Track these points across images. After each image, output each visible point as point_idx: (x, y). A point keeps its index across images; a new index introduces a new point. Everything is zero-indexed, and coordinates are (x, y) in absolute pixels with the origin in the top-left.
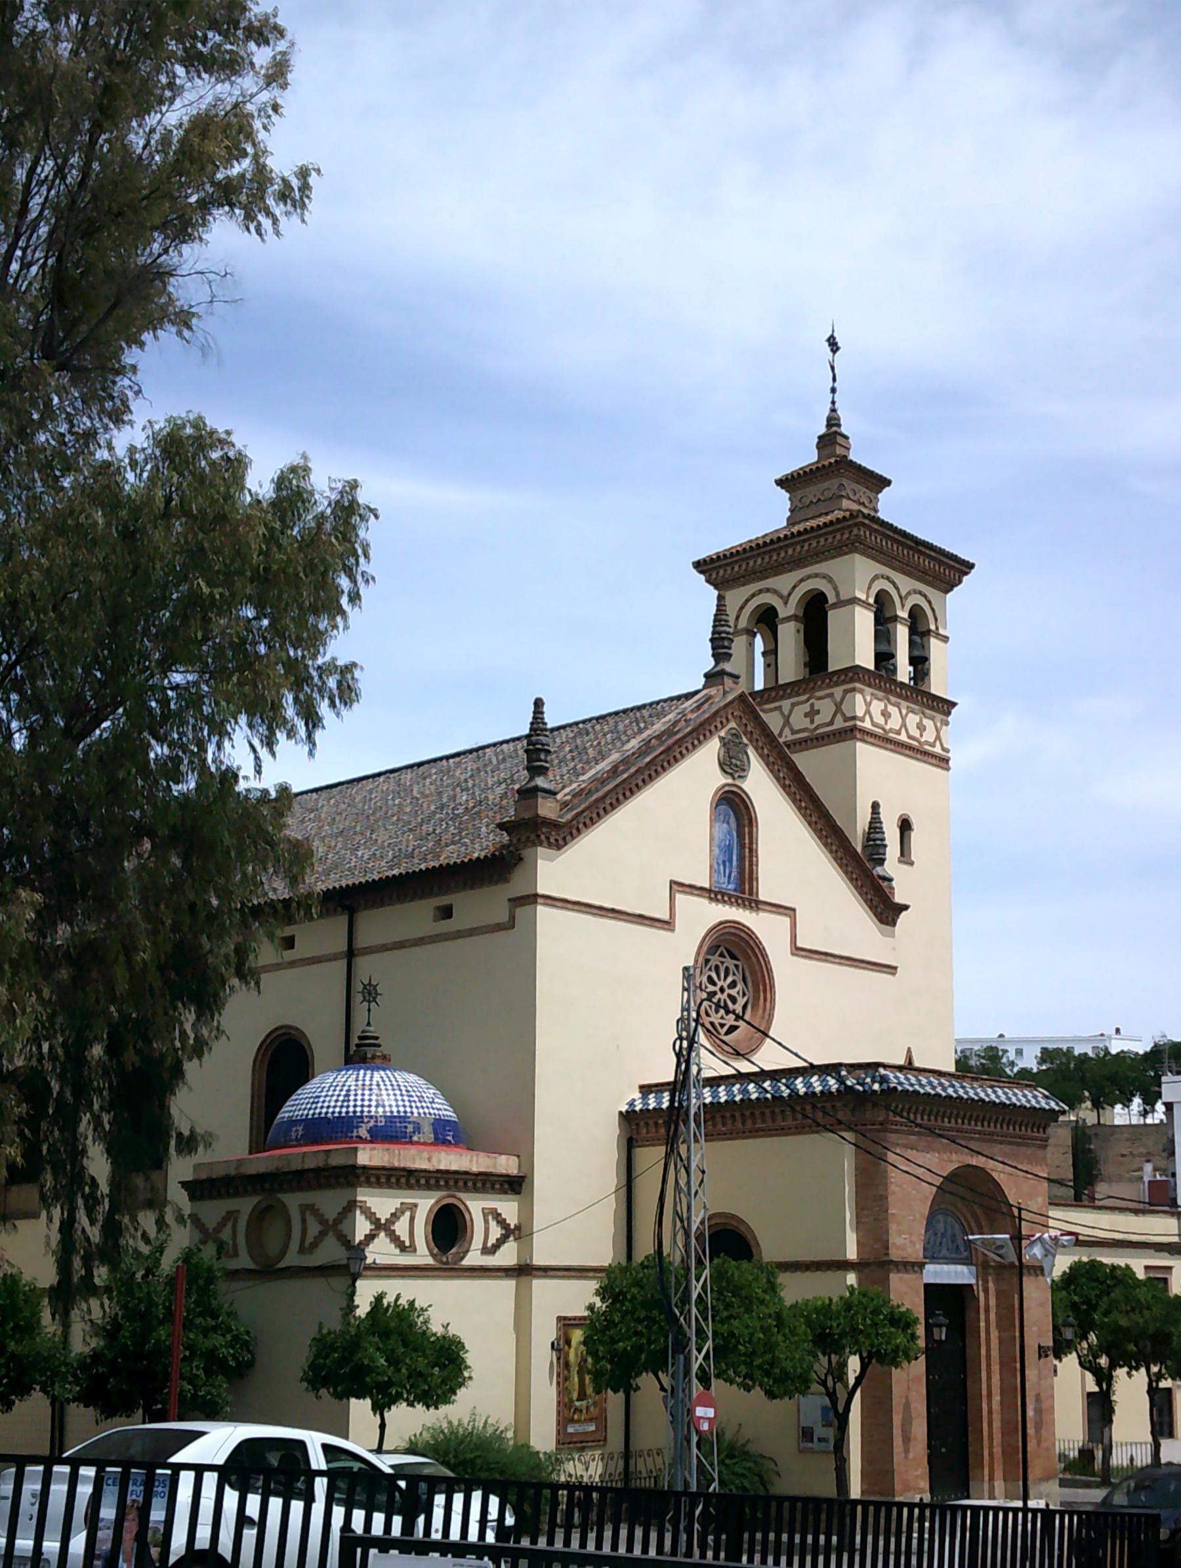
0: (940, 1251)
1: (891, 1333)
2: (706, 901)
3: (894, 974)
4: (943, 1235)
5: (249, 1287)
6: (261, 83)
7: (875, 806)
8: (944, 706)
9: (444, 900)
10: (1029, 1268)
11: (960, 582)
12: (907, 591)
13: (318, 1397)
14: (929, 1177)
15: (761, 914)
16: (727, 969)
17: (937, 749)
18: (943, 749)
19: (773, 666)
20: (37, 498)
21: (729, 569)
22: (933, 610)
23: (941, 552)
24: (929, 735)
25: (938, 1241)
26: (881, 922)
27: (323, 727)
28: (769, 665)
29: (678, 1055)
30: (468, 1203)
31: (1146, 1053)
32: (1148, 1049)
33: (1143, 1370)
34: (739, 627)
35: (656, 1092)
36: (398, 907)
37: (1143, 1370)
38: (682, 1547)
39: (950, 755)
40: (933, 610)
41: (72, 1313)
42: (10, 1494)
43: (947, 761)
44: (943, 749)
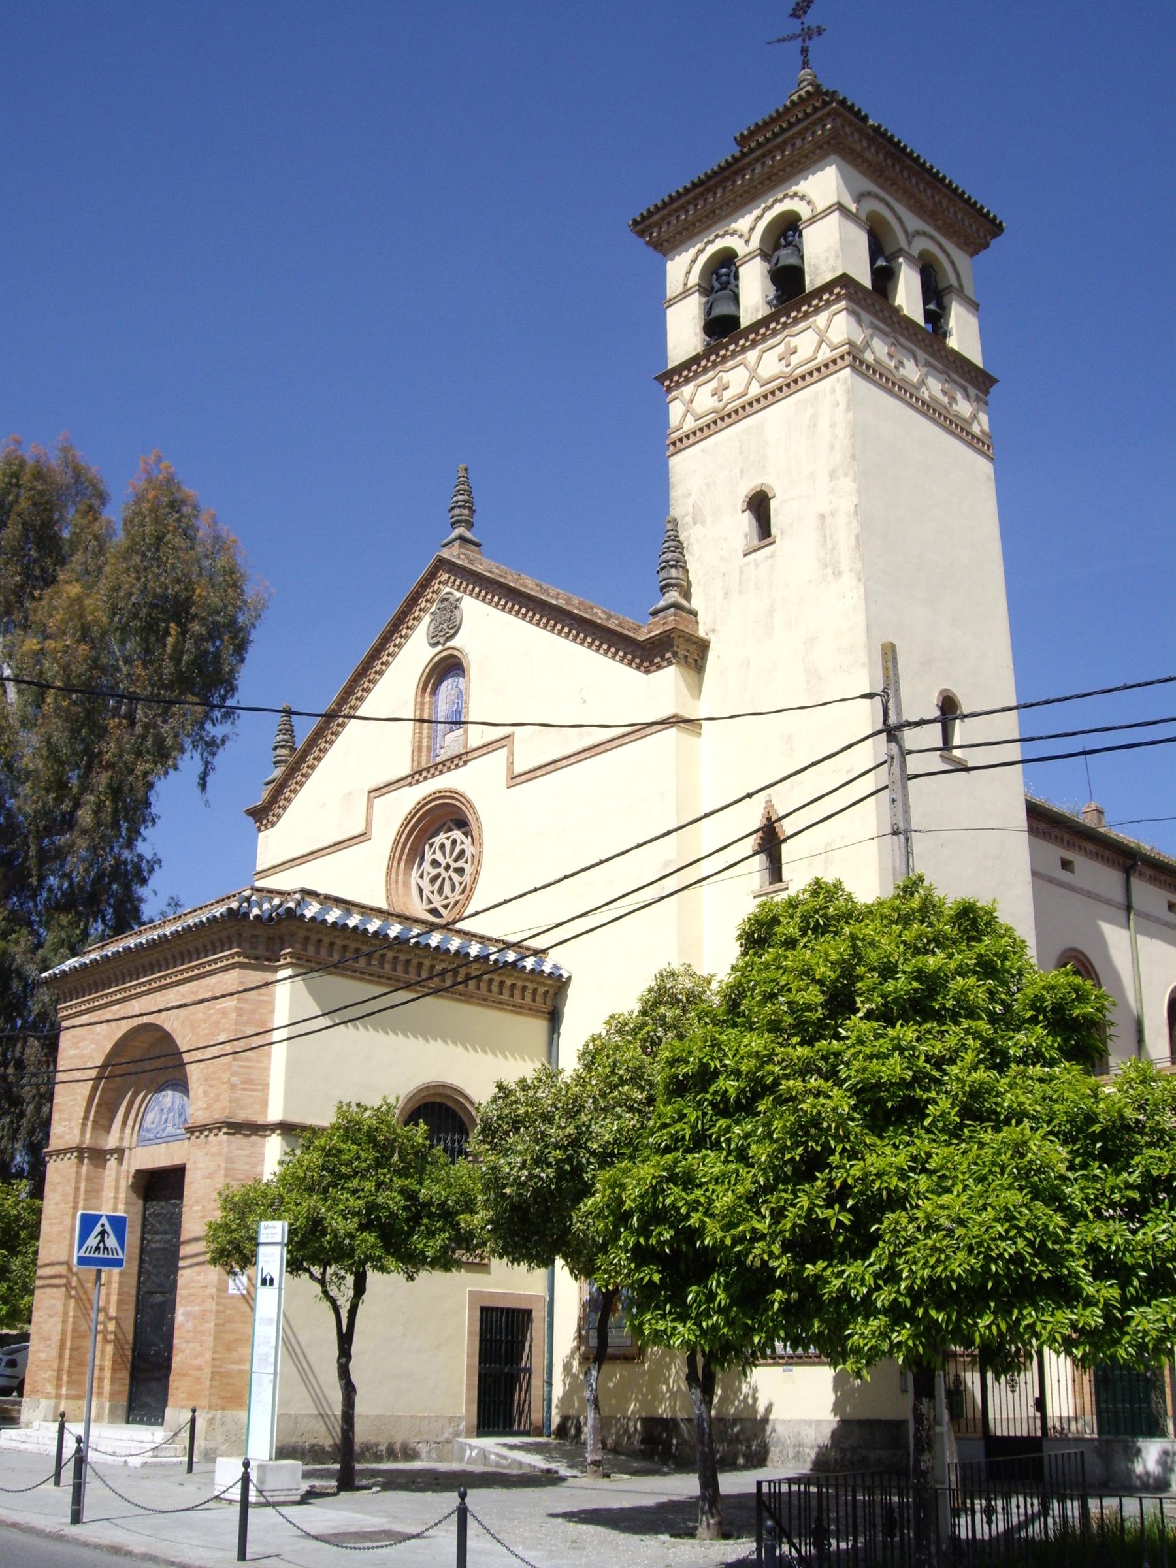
0: (164, 1130)
1: (344, 1142)
3: (239, 1559)
4: (170, 1110)
5: (386, 1546)
7: (755, 897)
9: (1069, 855)
10: (43, 693)
13: (769, 1409)
14: (198, 1055)
16: (463, 852)
19: (899, 804)
20: (69, 822)
21: (691, 207)
22: (953, 263)
23: (956, 194)
25: (164, 1117)
27: (411, 1278)
28: (894, 801)
29: (466, 763)
30: (754, 836)
32: (866, 236)
34: (690, 285)
35: (362, 914)
36: (519, 1490)
41: (445, 683)
42: (238, 1498)
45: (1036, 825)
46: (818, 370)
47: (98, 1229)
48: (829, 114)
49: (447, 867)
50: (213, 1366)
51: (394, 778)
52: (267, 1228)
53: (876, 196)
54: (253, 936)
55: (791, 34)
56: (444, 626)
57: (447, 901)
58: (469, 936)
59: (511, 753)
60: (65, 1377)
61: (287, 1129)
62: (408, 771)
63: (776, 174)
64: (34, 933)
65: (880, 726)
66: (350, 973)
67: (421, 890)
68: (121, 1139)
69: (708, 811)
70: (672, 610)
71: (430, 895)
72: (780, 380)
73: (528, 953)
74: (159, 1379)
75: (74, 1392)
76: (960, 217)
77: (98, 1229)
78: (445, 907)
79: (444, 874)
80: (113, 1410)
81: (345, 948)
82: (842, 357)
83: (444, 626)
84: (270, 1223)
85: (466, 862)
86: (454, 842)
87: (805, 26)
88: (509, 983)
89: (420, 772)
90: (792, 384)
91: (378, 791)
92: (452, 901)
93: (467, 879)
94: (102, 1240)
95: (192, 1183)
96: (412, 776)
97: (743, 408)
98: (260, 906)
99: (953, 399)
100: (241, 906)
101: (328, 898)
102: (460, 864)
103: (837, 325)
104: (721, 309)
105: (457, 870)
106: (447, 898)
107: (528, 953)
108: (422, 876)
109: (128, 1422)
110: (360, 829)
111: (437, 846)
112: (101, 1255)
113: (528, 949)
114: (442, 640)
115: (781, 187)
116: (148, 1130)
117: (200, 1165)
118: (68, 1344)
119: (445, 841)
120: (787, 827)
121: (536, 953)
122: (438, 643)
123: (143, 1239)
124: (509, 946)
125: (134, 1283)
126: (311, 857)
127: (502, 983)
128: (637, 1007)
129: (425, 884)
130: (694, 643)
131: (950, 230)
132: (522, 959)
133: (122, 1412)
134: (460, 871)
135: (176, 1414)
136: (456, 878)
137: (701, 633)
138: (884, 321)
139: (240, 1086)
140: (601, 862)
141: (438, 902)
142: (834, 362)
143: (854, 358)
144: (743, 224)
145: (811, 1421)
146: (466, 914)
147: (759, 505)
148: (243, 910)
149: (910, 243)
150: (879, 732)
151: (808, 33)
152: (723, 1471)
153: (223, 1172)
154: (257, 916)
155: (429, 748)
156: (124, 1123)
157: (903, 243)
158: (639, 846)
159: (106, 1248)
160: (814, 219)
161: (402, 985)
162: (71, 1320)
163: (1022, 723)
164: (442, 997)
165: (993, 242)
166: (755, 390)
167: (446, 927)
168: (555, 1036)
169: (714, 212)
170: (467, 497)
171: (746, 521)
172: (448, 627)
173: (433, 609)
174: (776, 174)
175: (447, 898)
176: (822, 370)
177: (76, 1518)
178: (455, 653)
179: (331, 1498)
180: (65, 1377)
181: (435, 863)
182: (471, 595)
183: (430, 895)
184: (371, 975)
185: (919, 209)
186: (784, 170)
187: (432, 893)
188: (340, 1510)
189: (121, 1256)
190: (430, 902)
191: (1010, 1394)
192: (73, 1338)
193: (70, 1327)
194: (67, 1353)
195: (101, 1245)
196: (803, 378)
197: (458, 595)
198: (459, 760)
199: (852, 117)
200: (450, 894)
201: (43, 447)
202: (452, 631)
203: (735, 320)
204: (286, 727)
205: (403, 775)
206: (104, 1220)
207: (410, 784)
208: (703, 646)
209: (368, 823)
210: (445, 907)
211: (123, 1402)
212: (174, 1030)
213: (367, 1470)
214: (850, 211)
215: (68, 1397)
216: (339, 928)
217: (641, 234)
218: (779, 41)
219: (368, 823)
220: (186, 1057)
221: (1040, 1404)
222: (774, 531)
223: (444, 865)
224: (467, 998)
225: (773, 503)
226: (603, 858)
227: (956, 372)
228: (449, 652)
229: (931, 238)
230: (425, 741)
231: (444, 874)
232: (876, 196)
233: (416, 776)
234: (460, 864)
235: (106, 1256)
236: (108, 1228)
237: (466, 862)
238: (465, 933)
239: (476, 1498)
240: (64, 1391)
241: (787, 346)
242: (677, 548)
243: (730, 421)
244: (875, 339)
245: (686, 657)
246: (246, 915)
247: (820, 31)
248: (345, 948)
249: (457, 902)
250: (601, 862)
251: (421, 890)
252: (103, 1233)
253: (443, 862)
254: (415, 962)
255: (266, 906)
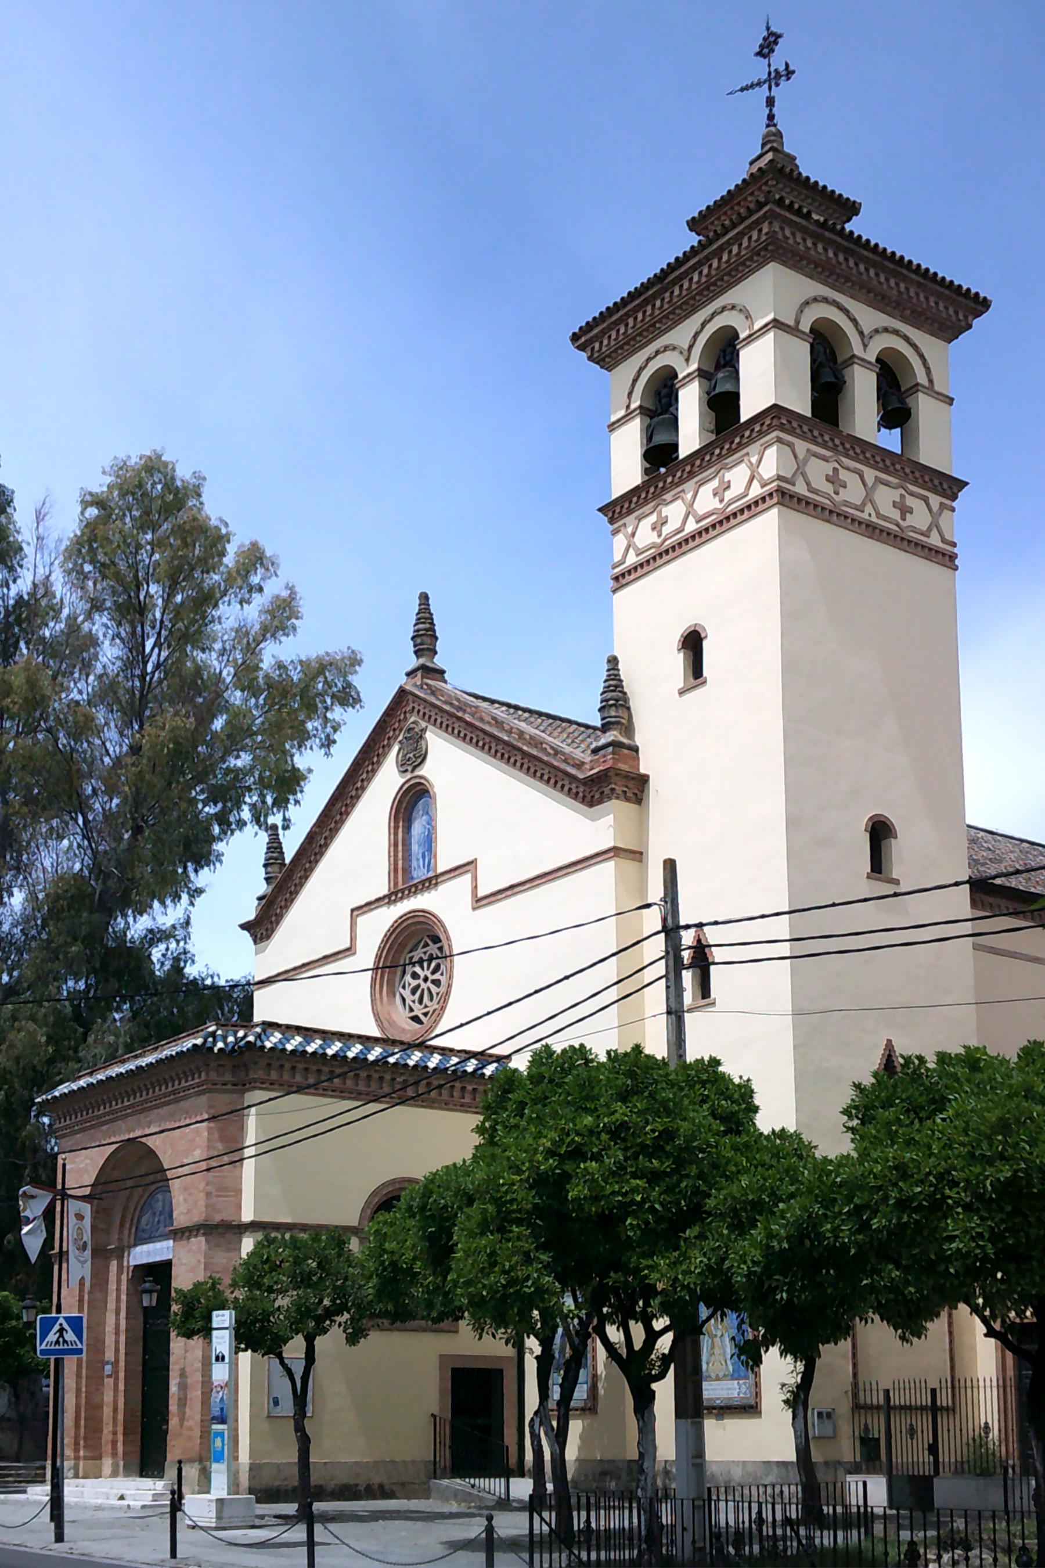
2: (385, 909)
6: (36, 582)
8: (949, 487)
11: (970, 327)
12: (869, 330)
15: (441, 888)
17: (934, 540)
18: (944, 540)
22: (922, 356)
24: (919, 518)
26: (591, 804)
30: (909, 386)
31: (843, 377)
33: (481, 1118)
37: (481, 1118)
38: (860, 1485)
39: (955, 550)
40: (922, 356)
43: (953, 557)
44: (944, 540)
45: (977, 896)
46: (853, 520)
47: (57, 1327)
48: (765, 217)
49: (426, 979)
50: (202, 1427)
51: (373, 898)
52: (217, 1316)
53: (826, 300)
54: (219, 1065)
55: (756, 81)
56: (411, 755)
57: (425, 950)
58: (446, 1052)
59: (475, 879)
60: (82, 1442)
61: (254, 1226)
62: (386, 892)
63: (714, 284)
64: (103, 809)
65: (660, 928)
66: (258, 1084)
67: (404, 1000)
68: (120, 1239)
69: (538, 988)
70: (610, 749)
71: (412, 1004)
72: (653, 550)
73: (490, 1059)
74: (235, 1249)
75: (90, 1454)
76: (941, 308)
77: (57, 1327)
78: (425, 1014)
79: (423, 985)
80: (126, 1467)
81: (319, 1071)
82: (771, 495)
83: (411, 755)
84: (220, 1312)
85: (442, 974)
86: (421, 1001)
87: (772, 69)
88: (470, 1088)
89: (395, 893)
90: (725, 521)
91: (358, 911)
92: (431, 1009)
93: (443, 989)
94: (61, 1335)
95: (177, 1276)
96: (388, 896)
97: (680, 544)
98: (224, 1038)
99: (558, 1370)
100: (205, 1041)
101: (289, 1027)
102: (437, 976)
103: (769, 461)
104: (660, 439)
105: (434, 982)
106: (426, 1006)
107: (490, 1059)
108: (404, 987)
109: (141, 1476)
110: (348, 945)
111: (308, 746)
112: (61, 1347)
113: (491, 1056)
114: (410, 768)
115: (164, 1111)
116: (143, 1231)
117: (184, 1261)
118: (83, 1415)
119: (429, 1004)
120: (718, 954)
121: (499, 1059)
122: (406, 771)
123: (145, 1324)
124: (474, 1055)
125: (140, 1361)
126: (509, 893)
127: (463, 1089)
128: (469, 1156)
129: (407, 993)
130: (633, 778)
131: (921, 319)
132: (483, 1067)
133: (136, 1467)
134: (437, 983)
135: (171, 1473)
136: (434, 989)
137: (643, 770)
138: (824, 445)
139: (215, 1193)
140: (462, 1025)
141: (418, 1011)
142: (763, 499)
143: (784, 496)
144: (681, 334)
145: (738, 1462)
146: (437, 1031)
147: (693, 643)
148: (208, 1045)
149: (865, 346)
150: (658, 933)
151: (775, 78)
152: (514, 1477)
153: (202, 1266)
154: (220, 1050)
155: (403, 869)
156: (122, 1225)
157: (857, 349)
158: (489, 1013)
159: (65, 1341)
160: (751, 338)
161: (294, 1089)
162: (84, 1395)
163: (243, 1154)
164: (409, 1105)
165: (976, 322)
166: (691, 526)
167: (421, 1046)
168: (418, 828)
169: (653, 325)
170: (428, 626)
171: (677, 662)
172: (414, 757)
173: (400, 738)
174: (714, 284)
175: (426, 1006)
176: (752, 509)
177: (59, 1538)
178: (422, 781)
179: (358, 1525)
180: (82, 1442)
181: (415, 976)
182: (435, 724)
183: (412, 1004)
184: (333, 1091)
185: (881, 302)
186: (722, 279)
187: (414, 1002)
188: (1003, 1387)
189: (80, 1346)
190: (411, 1010)
191: (909, 1440)
192: (86, 1409)
193: (83, 1402)
194: (82, 1422)
195: (61, 1340)
196: (735, 515)
197: (423, 724)
198: (431, 883)
199: (938, 287)
200: (429, 1004)
201: (10, 485)
202: (419, 760)
203: (675, 447)
204: (275, 845)
205: (381, 895)
206: (61, 1321)
207: (389, 903)
208: (644, 780)
209: (353, 939)
210: (425, 1014)
211: (136, 1459)
212: (156, 1147)
213: (753, 222)
214: (789, 326)
215: (85, 1458)
216: (299, 1054)
217: (582, 348)
218: (742, 90)
219: (353, 939)
220: (170, 1174)
221: (933, 1449)
222: (706, 672)
223: (422, 976)
224: (431, 1105)
225: (705, 643)
226: (464, 1022)
227: (915, 483)
228: (418, 780)
229: (896, 332)
230: (400, 863)
231: (423, 985)
232: (826, 300)
233: (392, 897)
234: (437, 976)
235: (66, 1347)
236: (66, 1326)
237: (442, 974)
238: (443, 1049)
239: (305, 1549)
240: (82, 1453)
241: (722, 481)
242: (616, 686)
243: (715, 533)
244: (774, 1351)
245: (625, 792)
246: (211, 1049)
247: (789, 73)
248: (319, 1071)
249: (434, 1011)
250: (462, 1025)
251: (404, 1000)
252: (61, 1330)
253: (429, 983)
254: (376, 1076)
255: (231, 1039)
